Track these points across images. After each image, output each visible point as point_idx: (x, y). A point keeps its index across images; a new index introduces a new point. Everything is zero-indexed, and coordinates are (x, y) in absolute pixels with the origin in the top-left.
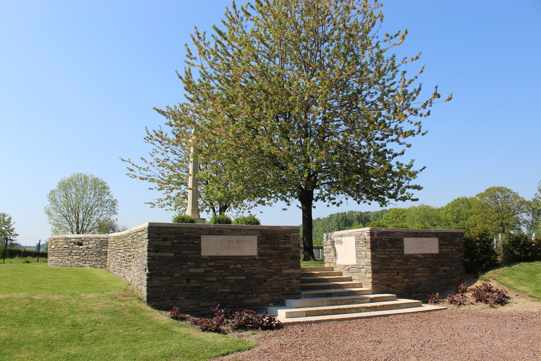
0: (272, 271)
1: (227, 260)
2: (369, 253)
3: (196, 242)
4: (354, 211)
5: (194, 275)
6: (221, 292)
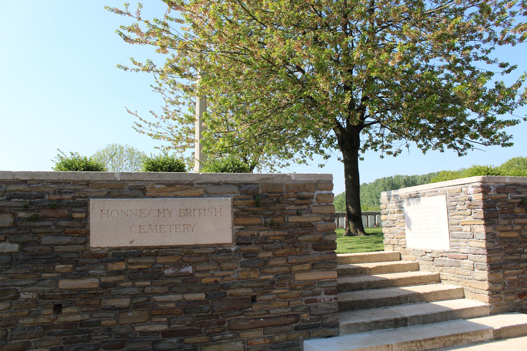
0: (271, 277)
1: (156, 255)
2: (481, 230)
3: (77, 215)
4: (401, 174)
5: (71, 296)
6: (144, 333)
